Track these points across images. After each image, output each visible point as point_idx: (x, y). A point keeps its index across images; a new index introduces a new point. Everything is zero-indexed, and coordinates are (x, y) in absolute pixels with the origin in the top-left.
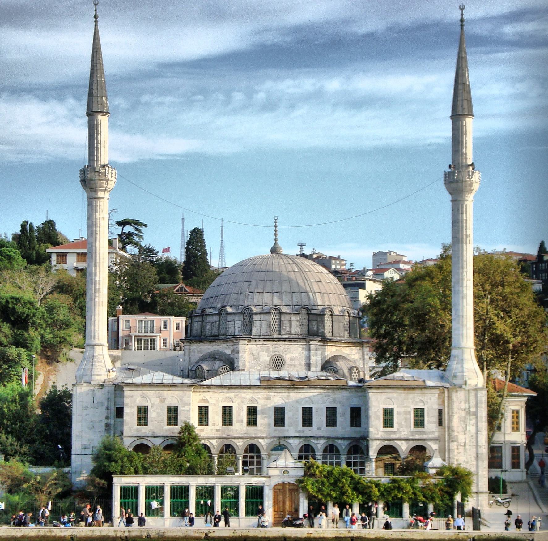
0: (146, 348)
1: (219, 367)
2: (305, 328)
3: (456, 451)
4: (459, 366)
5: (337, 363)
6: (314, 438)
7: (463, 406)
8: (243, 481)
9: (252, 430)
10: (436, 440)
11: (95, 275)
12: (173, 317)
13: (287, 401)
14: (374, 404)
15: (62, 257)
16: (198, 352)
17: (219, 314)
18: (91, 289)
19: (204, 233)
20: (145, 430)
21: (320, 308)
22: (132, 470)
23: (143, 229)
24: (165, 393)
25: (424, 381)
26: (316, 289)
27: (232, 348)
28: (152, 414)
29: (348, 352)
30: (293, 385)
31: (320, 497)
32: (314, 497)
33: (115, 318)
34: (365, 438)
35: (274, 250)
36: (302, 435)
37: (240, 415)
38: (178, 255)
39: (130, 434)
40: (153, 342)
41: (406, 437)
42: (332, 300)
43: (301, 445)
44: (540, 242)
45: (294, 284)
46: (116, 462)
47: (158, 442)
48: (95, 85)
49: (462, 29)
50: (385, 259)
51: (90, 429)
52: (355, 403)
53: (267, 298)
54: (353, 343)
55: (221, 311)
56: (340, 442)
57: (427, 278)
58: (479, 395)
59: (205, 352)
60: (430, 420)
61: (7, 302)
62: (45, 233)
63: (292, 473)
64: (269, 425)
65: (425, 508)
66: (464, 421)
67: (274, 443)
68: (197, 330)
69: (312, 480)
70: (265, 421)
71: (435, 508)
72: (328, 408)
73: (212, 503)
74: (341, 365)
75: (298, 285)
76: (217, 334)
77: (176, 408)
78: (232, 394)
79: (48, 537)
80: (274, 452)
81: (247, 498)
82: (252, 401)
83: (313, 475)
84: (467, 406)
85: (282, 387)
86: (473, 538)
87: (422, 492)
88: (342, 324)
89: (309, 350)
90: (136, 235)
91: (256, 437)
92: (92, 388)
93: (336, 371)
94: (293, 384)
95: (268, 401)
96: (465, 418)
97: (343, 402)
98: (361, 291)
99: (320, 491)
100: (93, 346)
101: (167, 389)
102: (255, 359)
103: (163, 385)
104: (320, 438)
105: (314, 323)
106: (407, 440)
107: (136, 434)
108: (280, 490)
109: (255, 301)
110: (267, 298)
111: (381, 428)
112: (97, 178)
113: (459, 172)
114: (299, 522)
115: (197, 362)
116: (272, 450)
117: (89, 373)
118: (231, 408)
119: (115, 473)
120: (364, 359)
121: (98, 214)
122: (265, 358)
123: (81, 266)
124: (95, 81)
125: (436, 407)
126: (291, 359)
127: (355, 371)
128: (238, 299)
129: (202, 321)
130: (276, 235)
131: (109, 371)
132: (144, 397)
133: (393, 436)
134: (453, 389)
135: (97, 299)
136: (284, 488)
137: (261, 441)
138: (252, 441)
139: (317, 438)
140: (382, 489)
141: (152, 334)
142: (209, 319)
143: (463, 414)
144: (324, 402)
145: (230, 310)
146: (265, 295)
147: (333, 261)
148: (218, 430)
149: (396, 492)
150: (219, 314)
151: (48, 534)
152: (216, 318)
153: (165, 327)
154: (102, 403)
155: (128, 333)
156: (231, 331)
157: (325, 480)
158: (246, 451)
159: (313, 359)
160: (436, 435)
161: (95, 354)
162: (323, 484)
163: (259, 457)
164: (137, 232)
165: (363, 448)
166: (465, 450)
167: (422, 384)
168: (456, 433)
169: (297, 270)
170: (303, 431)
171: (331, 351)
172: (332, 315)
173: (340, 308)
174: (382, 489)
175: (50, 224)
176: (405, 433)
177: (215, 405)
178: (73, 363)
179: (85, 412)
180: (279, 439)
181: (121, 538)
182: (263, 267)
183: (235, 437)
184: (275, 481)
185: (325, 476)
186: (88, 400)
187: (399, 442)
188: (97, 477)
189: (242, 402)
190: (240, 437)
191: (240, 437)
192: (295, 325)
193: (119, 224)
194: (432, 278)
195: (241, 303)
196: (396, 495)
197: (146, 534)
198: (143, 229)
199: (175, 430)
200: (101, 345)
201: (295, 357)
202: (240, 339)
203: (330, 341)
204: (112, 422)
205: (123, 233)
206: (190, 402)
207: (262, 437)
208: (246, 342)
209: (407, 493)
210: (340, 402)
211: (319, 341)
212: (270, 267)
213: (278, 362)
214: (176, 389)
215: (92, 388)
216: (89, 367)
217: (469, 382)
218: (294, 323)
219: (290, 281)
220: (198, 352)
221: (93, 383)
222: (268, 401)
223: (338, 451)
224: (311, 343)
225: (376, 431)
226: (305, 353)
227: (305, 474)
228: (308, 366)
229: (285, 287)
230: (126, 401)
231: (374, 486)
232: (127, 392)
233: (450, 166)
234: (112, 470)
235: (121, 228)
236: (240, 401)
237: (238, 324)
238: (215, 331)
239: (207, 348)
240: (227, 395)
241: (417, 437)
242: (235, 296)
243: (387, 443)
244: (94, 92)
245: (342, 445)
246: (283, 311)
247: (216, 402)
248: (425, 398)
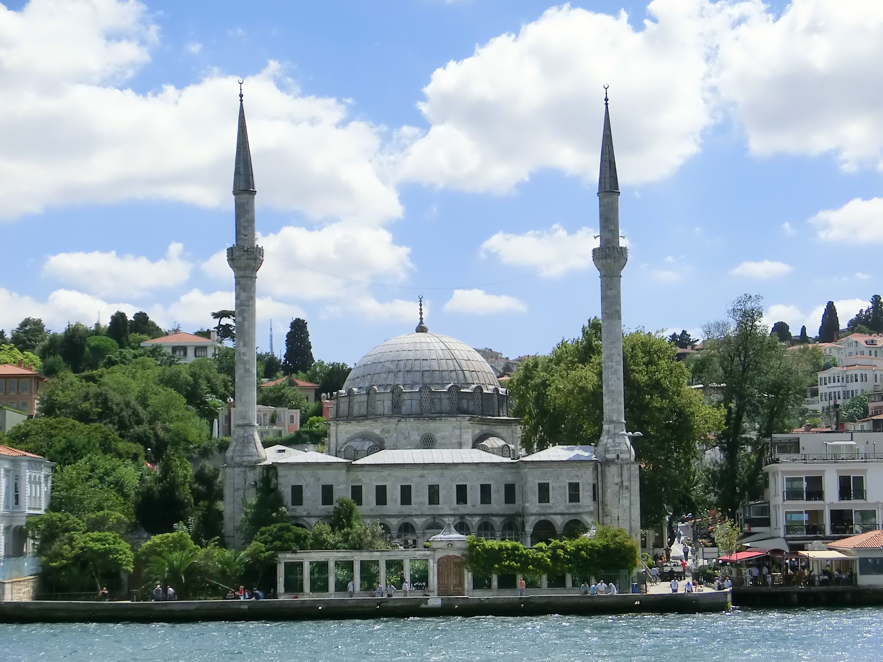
6: (468, 515)
9: (406, 509)
10: (591, 513)
16: (346, 433)
19: (309, 328)
28: (307, 494)
34: (522, 514)
36: (457, 512)
38: (280, 351)
41: (561, 511)
44: (777, 23)
52: (509, 479)
56: (494, 518)
60: (586, 495)
80: (428, 531)
84: (619, 480)
91: (410, 516)
96: (619, 492)
104: (476, 515)
106: (562, 514)
111: (537, 504)
125: (591, 481)
126: (443, 438)
129: (349, 402)
133: (549, 511)
137: (415, 520)
138: (407, 520)
148: (372, 510)
160: (592, 508)
165: (519, 525)
168: (609, 507)
170: (458, 509)
176: (561, 508)
180: (434, 518)
183: (390, 516)
184: (439, 555)
187: (554, 517)
193: (216, 315)
195: (389, 382)
205: (220, 326)
220: (346, 433)
223: (492, 528)
240: (381, 474)
241: (573, 511)
242: (384, 375)
245: (497, 522)
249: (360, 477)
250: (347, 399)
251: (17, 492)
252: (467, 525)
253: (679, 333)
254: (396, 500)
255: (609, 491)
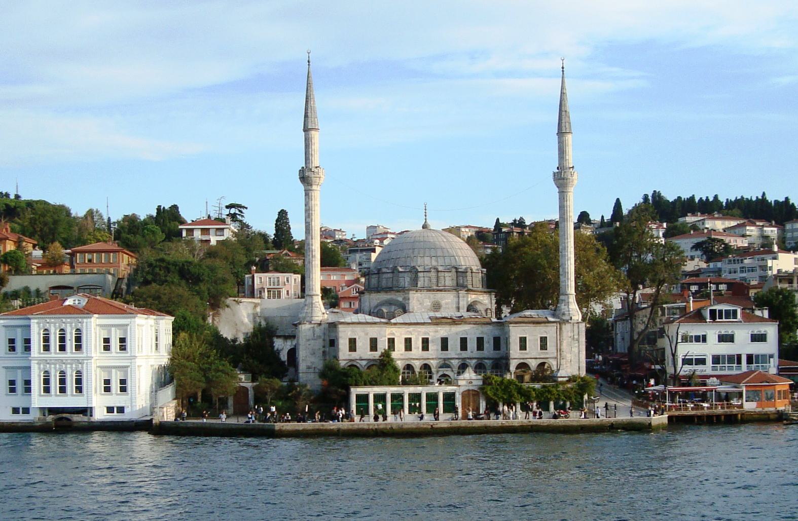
0: (274, 298)
1: (395, 310)
2: (455, 282)
3: (565, 365)
4: (566, 307)
5: (477, 306)
6: (468, 358)
7: (570, 334)
8: (441, 390)
9: (425, 354)
11: (312, 245)
12: (292, 274)
13: (449, 333)
14: (513, 334)
15: (190, 231)
17: (393, 272)
18: (309, 255)
20: (354, 355)
21: (464, 267)
22: (363, 383)
23: (244, 210)
24: (368, 329)
25: (546, 318)
26: (460, 254)
27: (403, 297)
28: (450, 344)
29: (482, 298)
30: (454, 322)
31: (496, 398)
32: (492, 399)
33: (251, 275)
34: (506, 358)
35: (425, 227)
36: (460, 357)
37: (417, 344)
39: (344, 358)
40: (279, 293)
42: (471, 262)
43: (460, 364)
44: (496, 219)
45: (445, 251)
46: (351, 377)
47: (364, 363)
48: (309, 110)
49: (563, 73)
50: (376, 231)
51: (312, 355)
52: (497, 333)
53: (427, 261)
54: (485, 292)
55: (394, 270)
56: (486, 361)
57: (527, 246)
58: (580, 326)
59: (382, 299)
61: (183, 264)
62: (173, 214)
63: (475, 383)
64: (437, 350)
65: (565, 404)
66: (570, 345)
67: (441, 363)
68: (374, 285)
69: (489, 387)
70: (435, 347)
71: (571, 404)
72: (478, 338)
73: (420, 405)
74: (479, 307)
75: (448, 251)
76: (391, 286)
77: (376, 339)
78: (411, 328)
79: (321, 430)
80: (440, 369)
81: (444, 400)
82: (425, 333)
83: (490, 384)
85: (446, 323)
86: (432, 426)
87: (563, 394)
88: (478, 279)
89: (459, 297)
90: (239, 215)
92: (312, 326)
93: (476, 311)
94: (454, 322)
95: (436, 333)
96: (571, 342)
97: (488, 333)
98: (372, 254)
99: (495, 394)
100: (311, 296)
101: (369, 326)
102: (420, 304)
103: (367, 323)
105: (461, 278)
107: (348, 357)
108: (466, 394)
109: (419, 263)
110: (427, 261)
112: (313, 176)
113: (565, 172)
114: (481, 416)
115: (377, 306)
116: (439, 368)
117: (310, 315)
118: (410, 339)
119: (351, 385)
120: (491, 303)
121: (313, 201)
122: (428, 303)
123: (205, 238)
124: (310, 107)
126: (446, 304)
127: (489, 311)
128: (406, 262)
129: (379, 277)
130: (426, 215)
131: (324, 314)
132: (353, 331)
134: (562, 323)
135: (314, 263)
136: (469, 394)
137: (432, 361)
139: (470, 359)
140: (537, 392)
141: (278, 287)
142: (385, 276)
143: (570, 340)
144: (475, 334)
145: (400, 270)
146: (426, 258)
147: (337, 233)
148: (402, 354)
149: (547, 394)
150: (393, 272)
151: (321, 428)
152: (390, 275)
153: (288, 281)
154: (320, 336)
155: (261, 286)
156: (402, 284)
157: (498, 387)
158: (404, 369)
159: (461, 303)
161: (314, 302)
162: (497, 390)
163: (430, 372)
164: (239, 213)
166: (571, 365)
167: (546, 320)
168: (565, 353)
169: (445, 240)
171: (472, 297)
172: (472, 272)
173: (476, 268)
174: (537, 392)
175: (175, 208)
177: (399, 337)
178: (229, 309)
179: (308, 343)
181: (372, 429)
182: (422, 239)
183: (414, 359)
184: (463, 389)
185: (498, 385)
186: (310, 334)
188: (339, 388)
189: (418, 334)
190: (417, 359)
191: (417, 359)
192: (448, 280)
193: (227, 207)
194: (530, 246)
195: (408, 265)
196: (547, 396)
197: (390, 426)
198: (244, 210)
199: (377, 355)
200: (317, 295)
201: (449, 303)
202: (409, 290)
203: (472, 291)
204: (327, 349)
206: (384, 333)
207: (433, 359)
208: (414, 292)
209: (554, 394)
210: (486, 334)
211: (466, 291)
212: (426, 239)
213: (437, 306)
214: (376, 326)
215: (312, 326)
216: (309, 311)
217: (573, 318)
218: (447, 278)
219: (442, 248)
221: (313, 322)
222: (436, 333)
223: (485, 368)
224: (460, 292)
225: (515, 353)
226: (456, 300)
227: (484, 383)
228: (458, 309)
229: (439, 253)
230: (341, 334)
231: (532, 390)
232: (341, 328)
233: (558, 168)
234: (349, 382)
235: (228, 210)
236: (416, 333)
237: (407, 279)
238: (390, 285)
239: (383, 297)
240: (408, 330)
243: (522, 361)
244: (309, 114)
245: (488, 363)
246: (440, 270)
247: (400, 335)
248: (549, 328)
249: (394, 332)
250: (377, 276)
251: (157, 340)
252: (484, 365)
253: (518, 219)
254: (418, 348)
255: (565, 342)
